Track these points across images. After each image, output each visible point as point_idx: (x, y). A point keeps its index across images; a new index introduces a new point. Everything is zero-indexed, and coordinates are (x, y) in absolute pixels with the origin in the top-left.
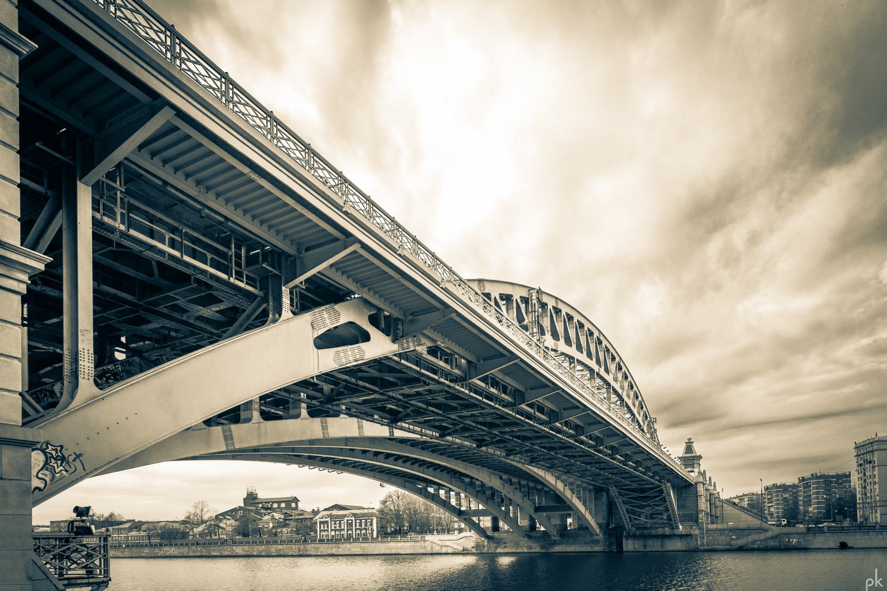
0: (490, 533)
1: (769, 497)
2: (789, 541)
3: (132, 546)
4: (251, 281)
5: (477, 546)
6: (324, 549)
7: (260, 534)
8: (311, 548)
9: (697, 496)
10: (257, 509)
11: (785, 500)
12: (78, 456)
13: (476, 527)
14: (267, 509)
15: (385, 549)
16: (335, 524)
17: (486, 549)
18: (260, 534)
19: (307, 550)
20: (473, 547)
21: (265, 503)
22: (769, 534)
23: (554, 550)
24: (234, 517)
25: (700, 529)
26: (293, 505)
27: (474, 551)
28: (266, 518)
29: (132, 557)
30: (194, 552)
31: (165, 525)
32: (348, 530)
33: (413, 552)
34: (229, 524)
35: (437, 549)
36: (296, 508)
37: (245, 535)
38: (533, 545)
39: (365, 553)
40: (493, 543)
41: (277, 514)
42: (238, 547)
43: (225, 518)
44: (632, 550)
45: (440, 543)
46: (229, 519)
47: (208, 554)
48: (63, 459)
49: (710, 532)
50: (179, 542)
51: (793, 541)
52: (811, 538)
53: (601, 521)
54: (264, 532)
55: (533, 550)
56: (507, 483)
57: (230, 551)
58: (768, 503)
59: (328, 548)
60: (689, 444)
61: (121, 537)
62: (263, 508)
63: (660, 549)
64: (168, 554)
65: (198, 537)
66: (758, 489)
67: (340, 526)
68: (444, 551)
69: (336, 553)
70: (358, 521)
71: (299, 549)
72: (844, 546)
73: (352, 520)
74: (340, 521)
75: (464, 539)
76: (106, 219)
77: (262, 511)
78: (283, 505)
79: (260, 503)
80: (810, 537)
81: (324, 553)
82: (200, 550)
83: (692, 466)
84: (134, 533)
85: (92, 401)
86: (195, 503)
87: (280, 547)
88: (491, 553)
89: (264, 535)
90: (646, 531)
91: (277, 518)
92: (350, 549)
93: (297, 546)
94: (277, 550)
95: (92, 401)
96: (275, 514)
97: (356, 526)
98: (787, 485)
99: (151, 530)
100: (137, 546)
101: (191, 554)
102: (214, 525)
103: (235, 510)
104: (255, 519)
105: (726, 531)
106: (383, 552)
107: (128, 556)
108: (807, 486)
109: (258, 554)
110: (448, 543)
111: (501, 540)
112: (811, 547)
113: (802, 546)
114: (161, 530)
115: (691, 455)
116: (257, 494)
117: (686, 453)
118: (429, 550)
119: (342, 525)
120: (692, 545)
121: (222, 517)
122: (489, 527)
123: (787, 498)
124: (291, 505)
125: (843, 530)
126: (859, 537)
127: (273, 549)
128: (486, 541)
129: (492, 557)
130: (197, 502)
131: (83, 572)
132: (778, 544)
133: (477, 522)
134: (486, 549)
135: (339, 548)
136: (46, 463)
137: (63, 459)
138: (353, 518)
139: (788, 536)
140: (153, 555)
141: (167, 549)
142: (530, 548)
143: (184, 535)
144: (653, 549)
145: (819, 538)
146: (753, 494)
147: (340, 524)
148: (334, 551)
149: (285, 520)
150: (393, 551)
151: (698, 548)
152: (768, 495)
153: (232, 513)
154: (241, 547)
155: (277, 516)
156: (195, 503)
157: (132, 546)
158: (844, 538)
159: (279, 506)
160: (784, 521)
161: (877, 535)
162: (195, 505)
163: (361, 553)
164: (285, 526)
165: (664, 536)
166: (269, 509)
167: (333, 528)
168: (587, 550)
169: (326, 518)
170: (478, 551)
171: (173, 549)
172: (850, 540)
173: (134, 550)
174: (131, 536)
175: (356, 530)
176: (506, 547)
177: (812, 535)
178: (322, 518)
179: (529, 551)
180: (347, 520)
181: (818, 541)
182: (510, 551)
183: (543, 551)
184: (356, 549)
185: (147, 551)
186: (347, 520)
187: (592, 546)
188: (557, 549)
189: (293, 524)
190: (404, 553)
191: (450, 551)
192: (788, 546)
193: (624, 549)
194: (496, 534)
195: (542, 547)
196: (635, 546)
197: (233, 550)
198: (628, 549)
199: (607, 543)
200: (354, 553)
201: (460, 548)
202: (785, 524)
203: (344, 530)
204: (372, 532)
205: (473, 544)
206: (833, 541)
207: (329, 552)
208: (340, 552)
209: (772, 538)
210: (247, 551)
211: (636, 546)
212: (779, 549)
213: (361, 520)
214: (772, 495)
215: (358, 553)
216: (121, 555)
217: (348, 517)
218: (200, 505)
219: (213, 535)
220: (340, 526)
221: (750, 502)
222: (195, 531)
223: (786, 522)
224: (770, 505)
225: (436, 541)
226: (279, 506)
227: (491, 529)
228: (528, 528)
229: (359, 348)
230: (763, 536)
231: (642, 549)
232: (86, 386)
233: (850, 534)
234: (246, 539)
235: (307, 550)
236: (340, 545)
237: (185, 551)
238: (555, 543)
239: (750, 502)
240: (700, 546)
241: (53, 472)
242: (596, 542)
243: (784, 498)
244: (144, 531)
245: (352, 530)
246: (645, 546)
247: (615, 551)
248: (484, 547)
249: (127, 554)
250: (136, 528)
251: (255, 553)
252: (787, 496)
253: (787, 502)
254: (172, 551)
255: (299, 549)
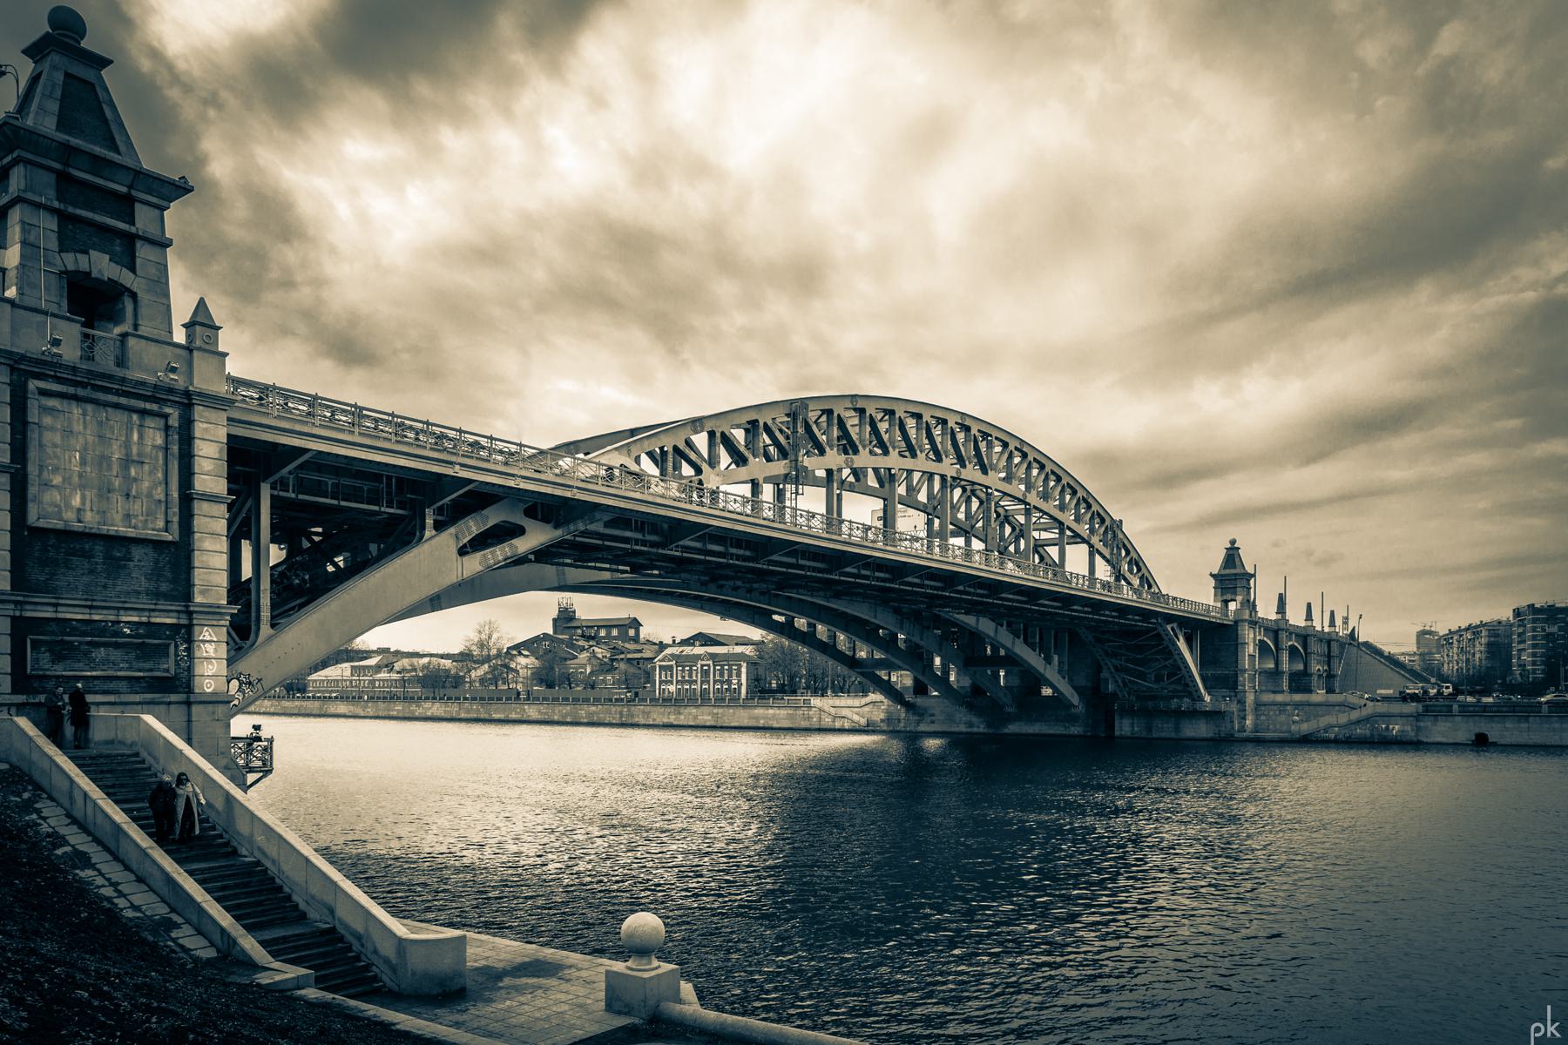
0: (909, 698)
1: (1521, 630)
2: (1387, 728)
3: (378, 698)
4: (401, 506)
5: (888, 720)
6: (660, 715)
7: (570, 685)
8: (639, 712)
9: (1237, 645)
10: (571, 639)
11: (1548, 636)
12: (260, 680)
13: (888, 689)
14: (589, 638)
15: (750, 718)
16: (683, 671)
17: (902, 725)
18: (570, 685)
19: (632, 716)
20: (882, 721)
21: (587, 627)
22: (1355, 715)
23: (1006, 731)
24: (533, 653)
25: (1239, 702)
26: (632, 632)
27: (884, 727)
28: (584, 656)
29: (377, 717)
30: (468, 711)
31: (429, 663)
32: (702, 683)
33: (791, 726)
34: (525, 663)
35: (827, 721)
36: (636, 639)
37: (550, 686)
38: (974, 719)
39: (719, 725)
40: (914, 714)
41: (600, 650)
42: (532, 706)
43: (520, 654)
44: (1129, 734)
45: (833, 711)
46: (526, 656)
47: (487, 716)
48: (250, 683)
49: (1263, 708)
50: (451, 692)
51: (1393, 729)
52: (1429, 724)
53: (1082, 682)
54: (576, 680)
55: (975, 730)
56: (908, 618)
57: (519, 713)
58: (1519, 643)
59: (663, 714)
60: (1231, 552)
61: (365, 680)
62: (583, 636)
63: (1173, 735)
64: (429, 714)
65: (477, 685)
66: (1505, 613)
67: (690, 676)
68: (838, 725)
69: (675, 723)
70: (718, 668)
71: (621, 713)
72: (1481, 743)
73: (708, 665)
74: (691, 666)
75: (871, 706)
76: (282, 494)
77: (581, 643)
78: (615, 632)
79: (578, 627)
80: (1426, 723)
81: (656, 723)
82: (476, 709)
83: (1234, 590)
84: (383, 675)
85: (270, 638)
86: (479, 624)
87: (594, 708)
88: (910, 732)
89: (577, 685)
90: (1150, 703)
91: (600, 656)
92: (696, 717)
93: (619, 709)
94: (590, 714)
95: (270, 638)
96: (596, 649)
97: (714, 676)
98: (1558, 608)
99: (409, 671)
100: (385, 698)
101: (463, 715)
102: (501, 665)
103: (536, 639)
104: (568, 656)
105: (1289, 708)
106: (746, 723)
107: (371, 714)
108: (1522, 624)
109: (561, 720)
110: (845, 712)
111: (925, 709)
112: (1425, 740)
113: (1408, 738)
114: (422, 671)
115: (1233, 571)
116: (574, 612)
117: (1225, 568)
118: (815, 722)
119: (694, 675)
120: (1224, 728)
121: (515, 652)
122: (908, 688)
123: (1553, 634)
124: (627, 633)
125: (1485, 712)
126: (1511, 726)
127: (583, 712)
128: (903, 710)
129: (912, 738)
130: (482, 622)
131: (260, 763)
132: (1368, 732)
133: (886, 678)
134: (902, 725)
135: (680, 714)
136: (240, 687)
137: (250, 683)
138: (711, 662)
139: (1386, 719)
140: (407, 715)
141: (427, 705)
142: (971, 725)
143: (457, 681)
144: (1163, 735)
145: (1443, 724)
146: (1500, 623)
147: (690, 671)
148: (672, 719)
149: (612, 660)
150: (762, 723)
151: (1232, 736)
152: (1519, 626)
153: (529, 645)
154: (536, 707)
155: (600, 652)
156: (479, 624)
157: (378, 698)
158: (1483, 726)
159: (609, 633)
160: (1447, 687)
161: (1519, 722)
162: (478, 627)
163: (713, 723)
164: (611, 669)
165: (1179, 715)
166: (593, 638)
167: (679, 678)
168: (1058, 732)
169: (670, 660)
170: (890, 728)
171: (437, 705)
172: (1494, 731)
173: (381, 705)
174: (379, 680)
175: (715, 682)
176: (933, 722)
177: (1432, 718)
178: (663, 660)
179: (969, 730)
180: (702, 666)
181: (1440, 730)
182: (939, 729)
183: (991, 731)
184: (705, 717)
185: (398, 708)
186: (702, 666)
187: (1067, 725)
188: (1013, 728)
189: (623, 666)
190: (777, 726)
191: (847, 725)
192: (1385, 737)
193: (1117, 733)
194: (920, 701)
195: (989, 726)
196: (1133, 727)
197: (524, 710)
198: (1123, 733)
199: (1090, 721)
200: (702, 724)
201: (863, 721)
202: (1450, 694)
203: (696, 681)
204: (740, 687)
205: (882, 716)
206: (1463, 731)
207: (666, 720)
208: (682, 720)
209: (1358, 722)
210: (546, 713)
211: (1136, 729)
212: (1370, 743)
213: (722, 666)
214: (1525, 626)
215: (708, 724)
216: (362, 714)
217: (702, 660)
218: (487, 628)
219: (500, 682)
220: (690, 676)
221: (1492, 639)
222: (473, 676)
223: (1451, 690)
224: (1521, 646)
225: (826, 708)
226: (609, 633)
227: (912, 690)
228: (969, 690)
229: (511, 545)
230: (1343, 719)
231: (1144, 734)
232: (265, 629)
233: (1496, 719)
234: (550, 693)
235: (632, 716)
236: (682, 710)
237: (453, 709)
238: (1010, 719)
239: (1492, 639)
240: (1239, 731)
241: (244, 693)
242: (1073, 719)
243: (1548, 634)
244: (398, 672)
245: (708, 682)
246: (1150, 730)
247: (1103, 735)
248: (899, 721)
249: (370, 711)
250: (387, 666)
251: (556, 718)
252: (1554, 629)
253: (1553, 642)
254: (436, 709)
255: (621, 713)
